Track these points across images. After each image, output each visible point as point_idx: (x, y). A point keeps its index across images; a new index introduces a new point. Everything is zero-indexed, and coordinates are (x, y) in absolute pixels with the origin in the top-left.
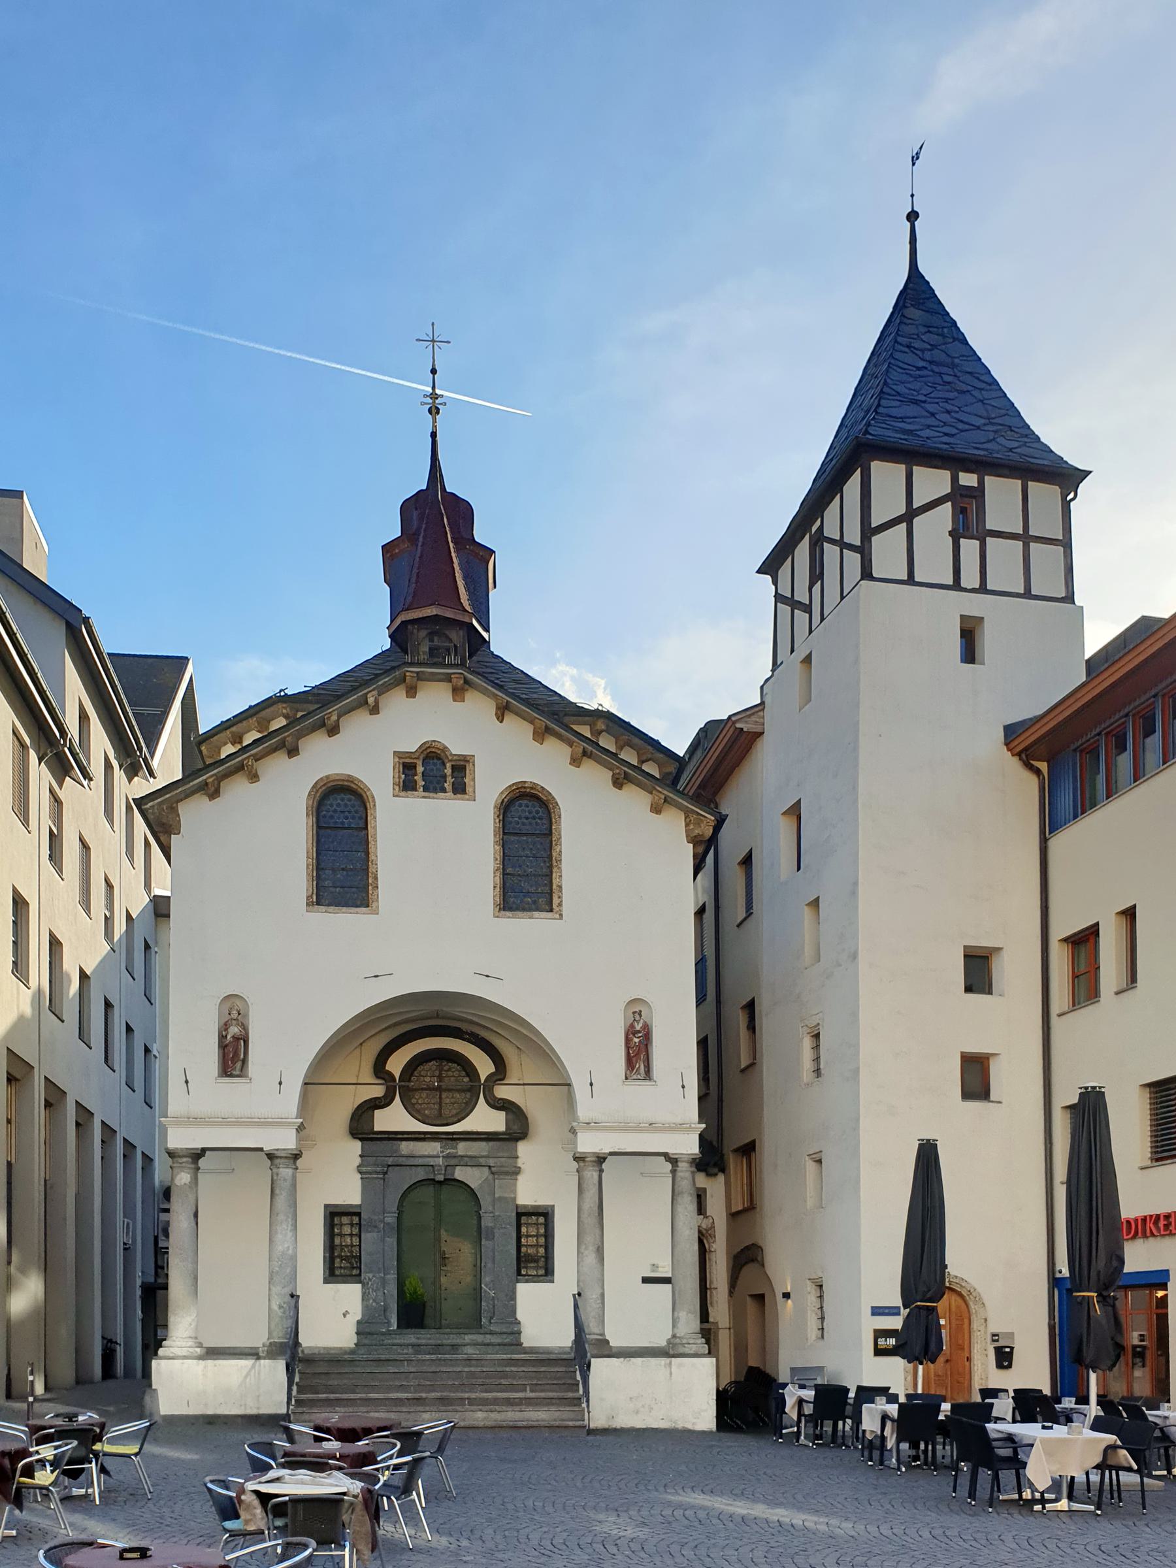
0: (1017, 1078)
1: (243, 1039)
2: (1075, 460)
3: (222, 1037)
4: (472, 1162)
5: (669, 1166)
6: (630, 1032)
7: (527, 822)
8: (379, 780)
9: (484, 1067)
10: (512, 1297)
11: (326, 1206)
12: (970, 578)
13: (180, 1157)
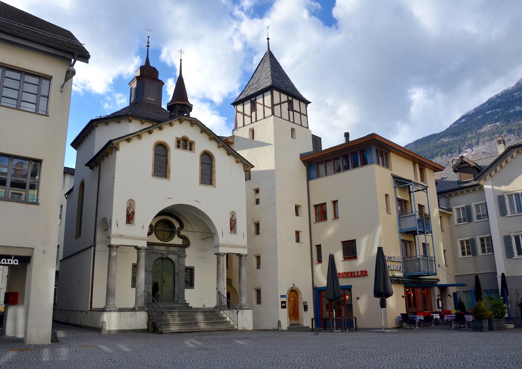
0: (305, 237)
1: (133, 213)
2: (308, 99)
3: (127, 212)
4: (173, 253)
5: (136, 251)
6: (128, 209)
7: (207, 159)
8: (172, 144)
9: (177, 225)
12: (292, 120)
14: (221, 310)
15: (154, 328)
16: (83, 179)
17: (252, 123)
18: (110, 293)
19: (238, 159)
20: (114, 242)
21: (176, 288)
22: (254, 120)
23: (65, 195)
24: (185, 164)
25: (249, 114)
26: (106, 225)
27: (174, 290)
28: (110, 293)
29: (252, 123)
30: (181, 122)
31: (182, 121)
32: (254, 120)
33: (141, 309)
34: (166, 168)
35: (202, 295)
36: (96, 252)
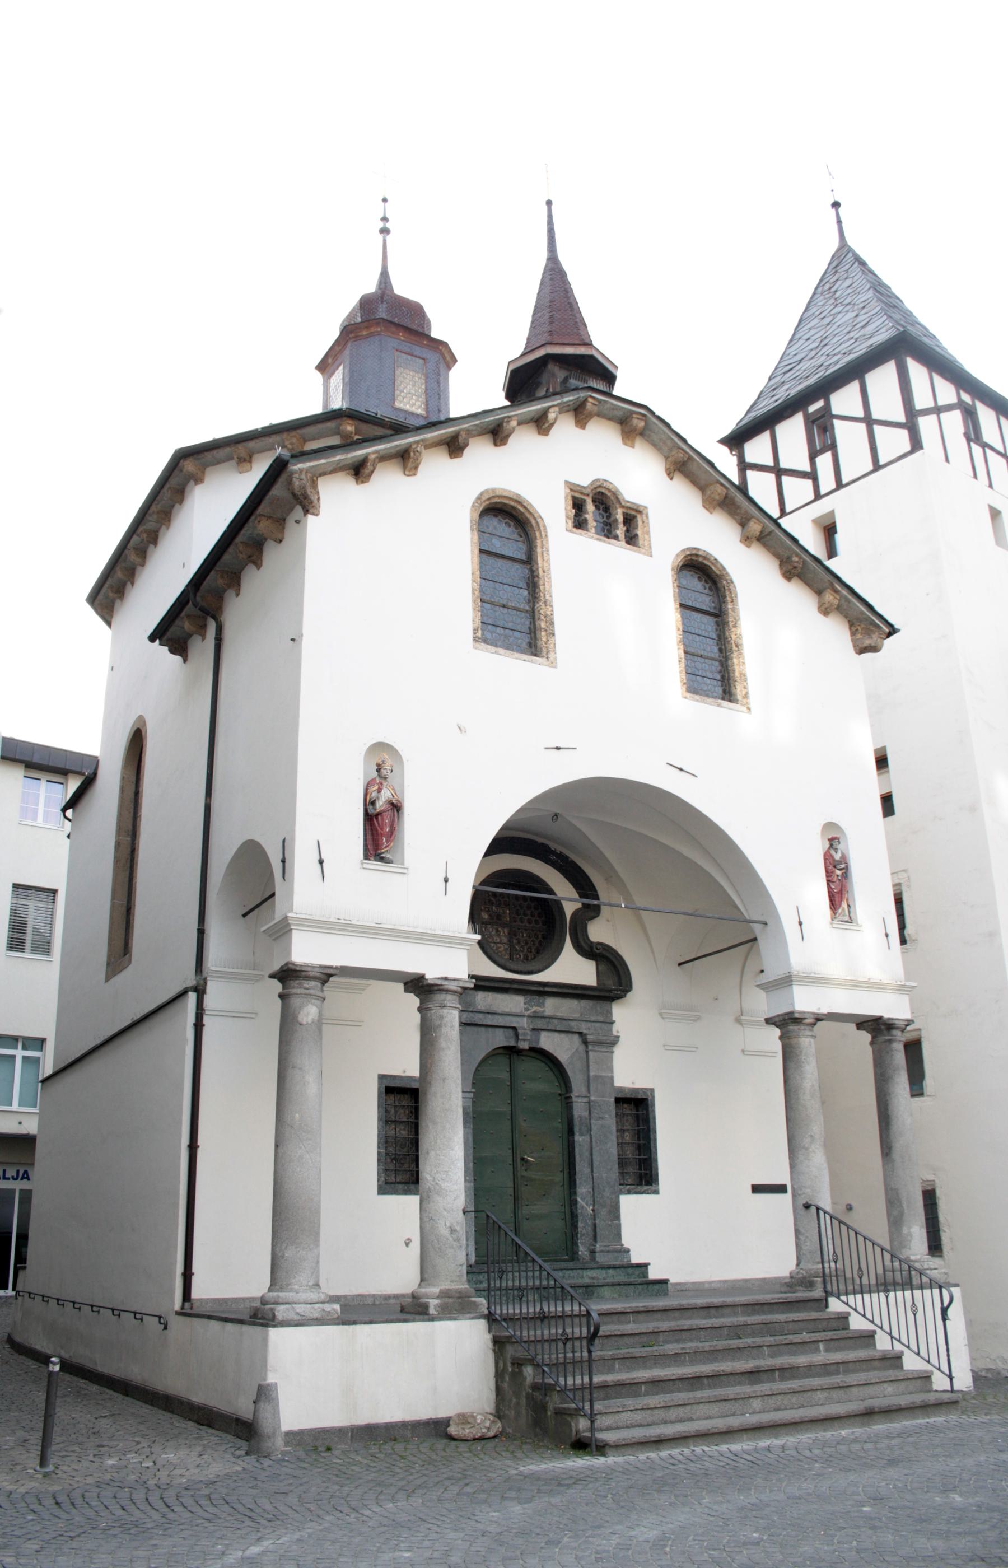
1: (396, 807)
3: (369, 803)
8: (551, 511)
10: (615, 1212)
11: (382, 1077)
13: (308, 978)
14: (828, 1294)
15: (541, 1407)
16: (141, 719)
17: (818, 496)
18: (290, 1220)
19: (829, 597)
20: (306, 950)
21: (583, 1190)
22: (827, 482)
23: (64, 810)
24: (611, 600)
25: (806, 467)
26: (256, 882)
27: (573, 1203)
28: (290, 1220)
29: (818, 496)
30: (580, 414)
31: (590, 416)
32: (827, 482)
33: (455, 1306)
34: (533, 614)
35: (705, 1220)
36: (206, 1020)
